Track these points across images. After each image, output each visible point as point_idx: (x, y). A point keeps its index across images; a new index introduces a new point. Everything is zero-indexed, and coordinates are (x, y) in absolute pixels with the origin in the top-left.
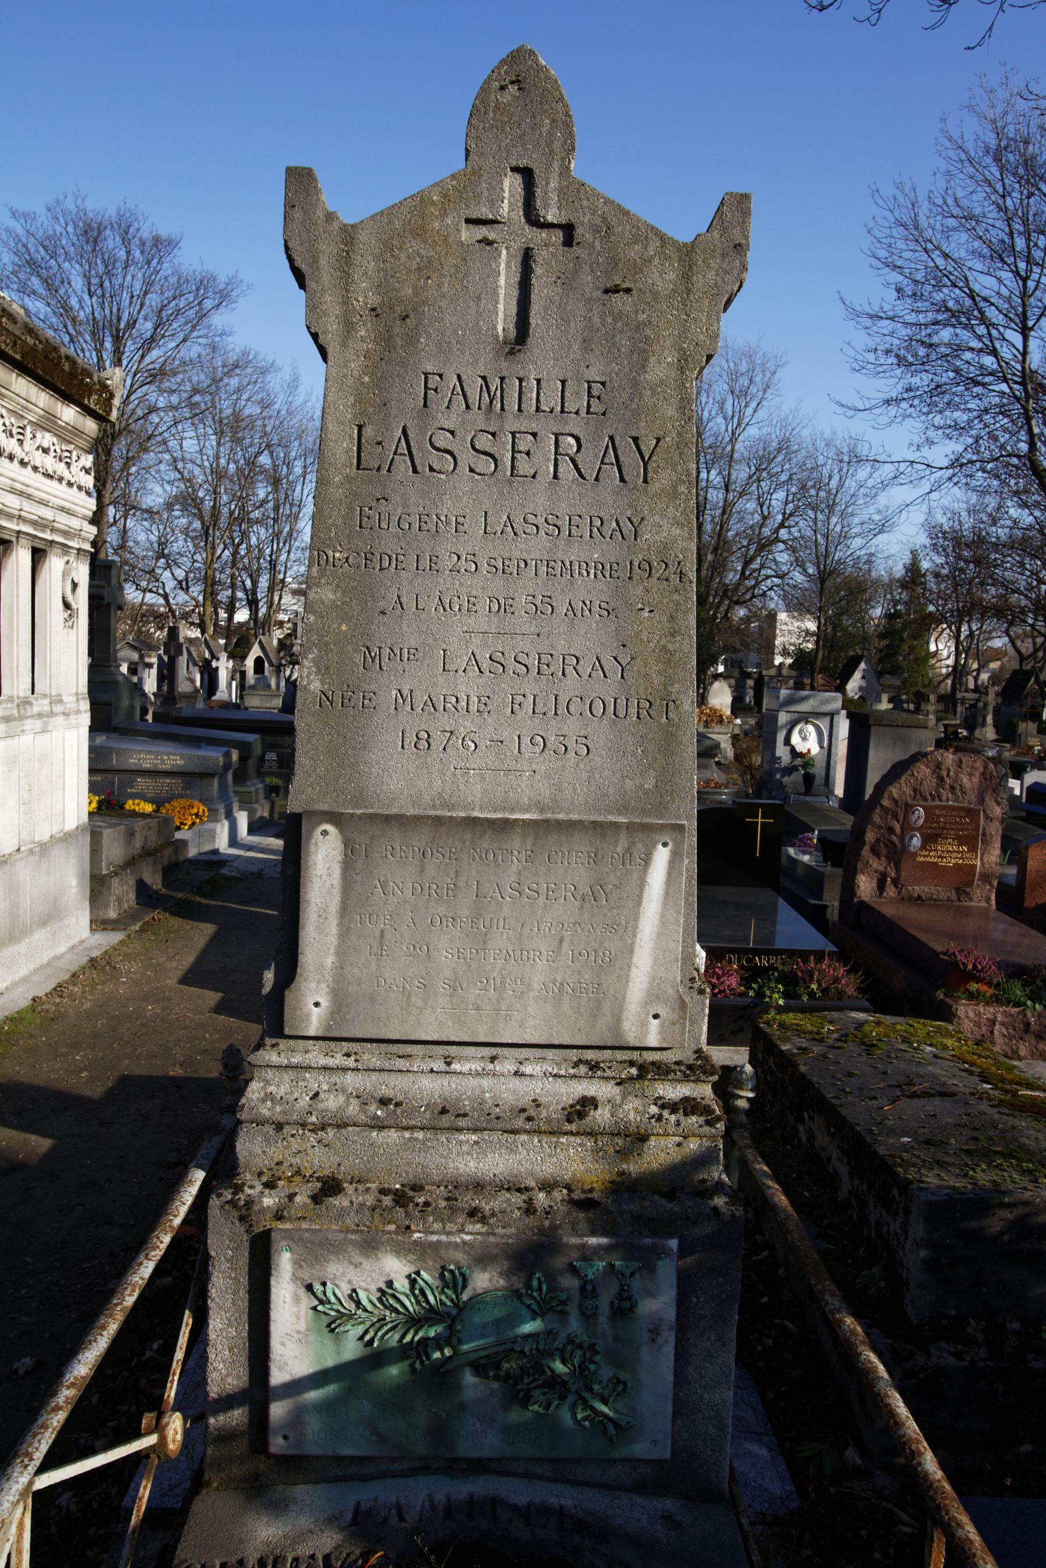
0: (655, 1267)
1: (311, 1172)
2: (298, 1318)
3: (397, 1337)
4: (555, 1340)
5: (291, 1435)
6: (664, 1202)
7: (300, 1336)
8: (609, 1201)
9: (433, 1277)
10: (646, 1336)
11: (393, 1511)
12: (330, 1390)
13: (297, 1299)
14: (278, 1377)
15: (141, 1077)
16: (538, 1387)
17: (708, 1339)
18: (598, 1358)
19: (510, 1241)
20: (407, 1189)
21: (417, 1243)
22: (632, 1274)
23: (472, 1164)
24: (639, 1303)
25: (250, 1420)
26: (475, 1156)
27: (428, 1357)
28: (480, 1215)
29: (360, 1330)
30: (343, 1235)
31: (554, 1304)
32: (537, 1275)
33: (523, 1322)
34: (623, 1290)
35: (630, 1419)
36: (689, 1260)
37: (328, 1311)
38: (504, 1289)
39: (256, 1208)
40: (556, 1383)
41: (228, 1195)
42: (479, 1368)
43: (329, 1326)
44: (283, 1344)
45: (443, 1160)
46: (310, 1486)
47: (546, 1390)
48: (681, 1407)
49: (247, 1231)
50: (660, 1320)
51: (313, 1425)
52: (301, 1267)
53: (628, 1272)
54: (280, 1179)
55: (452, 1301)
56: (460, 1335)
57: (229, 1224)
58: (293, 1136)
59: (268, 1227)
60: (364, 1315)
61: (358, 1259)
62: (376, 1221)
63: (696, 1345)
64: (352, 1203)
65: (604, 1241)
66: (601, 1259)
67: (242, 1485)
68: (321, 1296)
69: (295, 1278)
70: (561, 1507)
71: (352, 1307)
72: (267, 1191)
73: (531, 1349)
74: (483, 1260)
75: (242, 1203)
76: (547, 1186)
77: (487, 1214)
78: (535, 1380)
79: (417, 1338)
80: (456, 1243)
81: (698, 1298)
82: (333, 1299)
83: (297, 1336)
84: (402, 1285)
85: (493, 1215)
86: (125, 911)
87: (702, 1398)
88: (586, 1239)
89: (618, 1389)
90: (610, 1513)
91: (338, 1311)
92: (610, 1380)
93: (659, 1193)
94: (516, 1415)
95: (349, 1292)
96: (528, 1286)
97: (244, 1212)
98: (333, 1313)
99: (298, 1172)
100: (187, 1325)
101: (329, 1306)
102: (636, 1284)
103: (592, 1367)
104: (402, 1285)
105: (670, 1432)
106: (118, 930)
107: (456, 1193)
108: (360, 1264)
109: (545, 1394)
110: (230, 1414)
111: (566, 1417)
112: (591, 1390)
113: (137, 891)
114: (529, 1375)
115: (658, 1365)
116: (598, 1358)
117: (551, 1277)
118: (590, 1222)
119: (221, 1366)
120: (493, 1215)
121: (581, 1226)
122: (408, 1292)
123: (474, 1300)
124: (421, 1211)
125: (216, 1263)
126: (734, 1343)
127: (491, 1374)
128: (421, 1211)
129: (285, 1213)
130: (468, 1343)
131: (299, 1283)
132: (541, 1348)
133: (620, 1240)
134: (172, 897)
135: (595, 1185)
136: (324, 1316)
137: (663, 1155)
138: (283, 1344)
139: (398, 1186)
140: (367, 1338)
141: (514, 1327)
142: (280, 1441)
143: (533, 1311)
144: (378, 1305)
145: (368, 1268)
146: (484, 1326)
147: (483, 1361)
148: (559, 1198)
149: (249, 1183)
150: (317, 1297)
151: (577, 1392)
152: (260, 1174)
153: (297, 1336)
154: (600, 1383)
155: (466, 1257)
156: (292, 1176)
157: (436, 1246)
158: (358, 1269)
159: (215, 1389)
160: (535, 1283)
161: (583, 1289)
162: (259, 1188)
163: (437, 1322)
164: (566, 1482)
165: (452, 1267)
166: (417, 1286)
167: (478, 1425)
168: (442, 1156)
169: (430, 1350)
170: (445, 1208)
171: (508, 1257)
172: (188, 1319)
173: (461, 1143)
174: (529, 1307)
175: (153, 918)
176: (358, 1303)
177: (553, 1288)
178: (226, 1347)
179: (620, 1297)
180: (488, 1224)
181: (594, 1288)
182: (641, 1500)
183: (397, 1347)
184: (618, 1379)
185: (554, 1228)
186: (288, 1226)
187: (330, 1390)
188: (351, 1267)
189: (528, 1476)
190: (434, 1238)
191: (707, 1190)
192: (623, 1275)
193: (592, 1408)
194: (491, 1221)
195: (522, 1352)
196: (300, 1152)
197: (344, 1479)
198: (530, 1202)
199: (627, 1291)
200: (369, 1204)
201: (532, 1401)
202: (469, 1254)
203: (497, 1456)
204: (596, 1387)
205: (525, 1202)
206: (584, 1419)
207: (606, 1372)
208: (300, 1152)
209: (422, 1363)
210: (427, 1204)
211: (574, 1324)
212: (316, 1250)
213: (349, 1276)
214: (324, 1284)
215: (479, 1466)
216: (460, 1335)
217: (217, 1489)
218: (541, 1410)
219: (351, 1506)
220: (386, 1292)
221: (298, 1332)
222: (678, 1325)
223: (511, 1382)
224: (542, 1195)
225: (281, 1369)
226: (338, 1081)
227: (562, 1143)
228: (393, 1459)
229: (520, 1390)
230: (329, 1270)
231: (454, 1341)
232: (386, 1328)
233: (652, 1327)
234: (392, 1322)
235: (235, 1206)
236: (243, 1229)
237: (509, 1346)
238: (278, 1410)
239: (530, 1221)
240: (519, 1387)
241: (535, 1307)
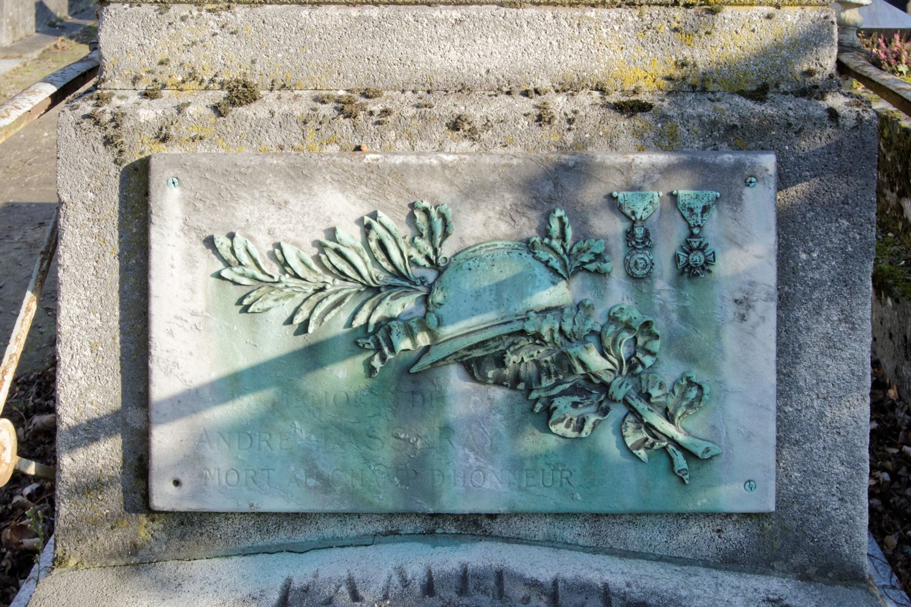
0: (740, 198)
1: (213, 73)
2: (193, 291)
3: (344, 317)
4: (588, 317)
5: (184, 480)
6: (750, 104)
7: (196, 320)
8: (665, 104)
9: (398, 222)
10: (731, 310)
11: (343, 589)
12: (246, 405)
13: (191, 262)
14: (163, 387)
15: (29, 205)
16: (563, 393)
17: (828, 320)
18: (655, 346)
19: (515, 161)
20: (356, 96)
21: (370, 168)
22: (705, 209)
23: (453, 55)
24: (718, 256)
25: (124, 460)
26: (457, 43)
27: (392, 349)
28: (467, 127)
29: (287, 308)
30: (259, 159)
31: (585, 259)
32: (559, 213)
33: (536, 288)
34: (692, 235)
35: (710, 445)
36: (792, 191)
37: (238, 279)
38: (508, 237)
39: (127, 124)
40: (593, 389)
41: (87, 107)
42: (475, 362)
43: (240, 302)
44: (171, 333)
45: (409, 50)
46: (216, 561)
47: (576, 399)
48: (787, 433)
49: (115, 162)
50: (752, 284)
51: (220, 461)
52: (196, 210)
53: (698, 206)
54: (164, 86)
55: (427, 258)
56: (441, 311)
57: (89, 151)
58: (183, 19)
59: (147, 154)
60: (294, 282)
61: (283, 195)
62: (309, 140)
63: (808, 329)
64: (272, 114)
65: (661, 159)
66: (655, 186)
67: (113, 563)
68: (227, 255)
69: (188, 227)
70: (606, 585)
71: (274, 270)
72: (146, 102)
73: (552, 330)
74: (475, 192)
75: (107, 117)
76: (568, 88)
77: (478, 125)
78: (558, 383)
79: (374, 320)
80: (431, 166)
81: (809, 252)
82: (245, 259)
83: (192, 320)
84: (350, 235)
85: (487, 126)
86: (21, 39)
87: (821, 415)
88: (631, 156)
89: (693, 393)
90: (684, 593)
91: (254, 278)
92: (676, 383)
93: (742, 93)
94: (535, 442)
95: (270, 248)
96: (546, 233)
97: (110, 131)
98: (245, 281)
99: (192, 76)
100: (28, 310)
101: (239, 270)
102: (713, 228)
103: (648, 360)
104: (350, 235)
105: (773, 465)
106: (11, 58)
107: (430, 99)
108: (286, 203)
109: (575, 405)
110: (94, 448)
111: (608, 441)
112: (647, 397)
113: (37, 15)
114: (549, 375)
115: (747, 358)
116: (655, 346)
117: (580, 218)
118: (638, 134)
119: (80, 374)
120: (487, 126)
121: (622, 140)
122: (359, 245)
123: (461, 256)
124: (378, 123)
125: (70, 212)
126: (868, 326)
127: (490, 374)
128: (378, 123)
129: (172, 131)
130: (453, 323)
131: (193, 235)
132: (567, 328)
133: (684, 157)
134: (80, 25)
135: (642, 83)
136: (231, 287)
137: (745, 33)
138: (171, 333)
139: (341, 92)
140: (299, 319)
141: (523, 296)
142: (170, 488)
143: (554, 271)
144: (314, 266)
145: (297, 209)
146: (478, 295)
147: (478, 353)
148: (588, 102)
149: (120, 93)
150: (221, 258)
151: (625, 402)
152: (136, 80)
153: (192, 320)
154: (661, 386)
155: (447, 188)
156: (183, 82)
157: (401, 172)
158: (283, 212)
159: (71, 411)
160: (555, 226)
161: (629, 235)
162: (134, 97)
163: (407, 291)
164: (611, 552)
165: (426, 204)
166: (373, 235)
167: (472, 460)
168: (408, 44)
169: (394, 337)
170: (414, 117)
171: (511, 185)
172: (30, 305)
173: (435, 22)
174: (546, 263)
175: (56, 46)
176: (284, 264)
177: (584, 234)
178: (86, 344)
179: (689, 249)
180: (479, 140)
181: (647, 235)
182: (730, 579)
183: (347, 334)
184: (689, 380)
185: (580, 144)
186: (176, 150)
187: (246, 405)
188: (272, 208)
189: (551, 543)
190: (398, 160)
191: (816, 87)
192: (691, 210)
193: (649, 427)
194: (485, 136)
195: (537, 336)
196: (194, 43)
197: (268, 551)
198: (543, 107)
199: (697, 236)
200: (297, 113)
201: (555, 416)
202: (452, 184)
203: (503, 509)
204: (655, 392)
205: (536, 107)
206: (641, 444)
207: (670, 370)
208: (194, 43)
209: (383, 359)
210: (386, 112)
211: (618, 294)
212: (219, 184)
213: (268, 224)
214: (231, 236)
215: (474, 526)
216: (441, 311)
217: (76, 568)
218: (570, 433)
219: (279, 583)
220: (327, 245)
221: (194, 314)
222: (780, 297)
223: (521, 386)
224: (561, 99)
225: (168, 372)
226: (349, 531)
227: (589, 19)
228: (342, 516)
229: (537, 400)
230: (238, 214)
231: (432, 320)
232: (326, 303)
233: (739, 296)
234: (337, 292)
235: (97, 123)
236: (109, 158)
237: (517, 326)
238: (165, 440)
239: (547, 134)
240: (534, 395)
241: (557, 265)
